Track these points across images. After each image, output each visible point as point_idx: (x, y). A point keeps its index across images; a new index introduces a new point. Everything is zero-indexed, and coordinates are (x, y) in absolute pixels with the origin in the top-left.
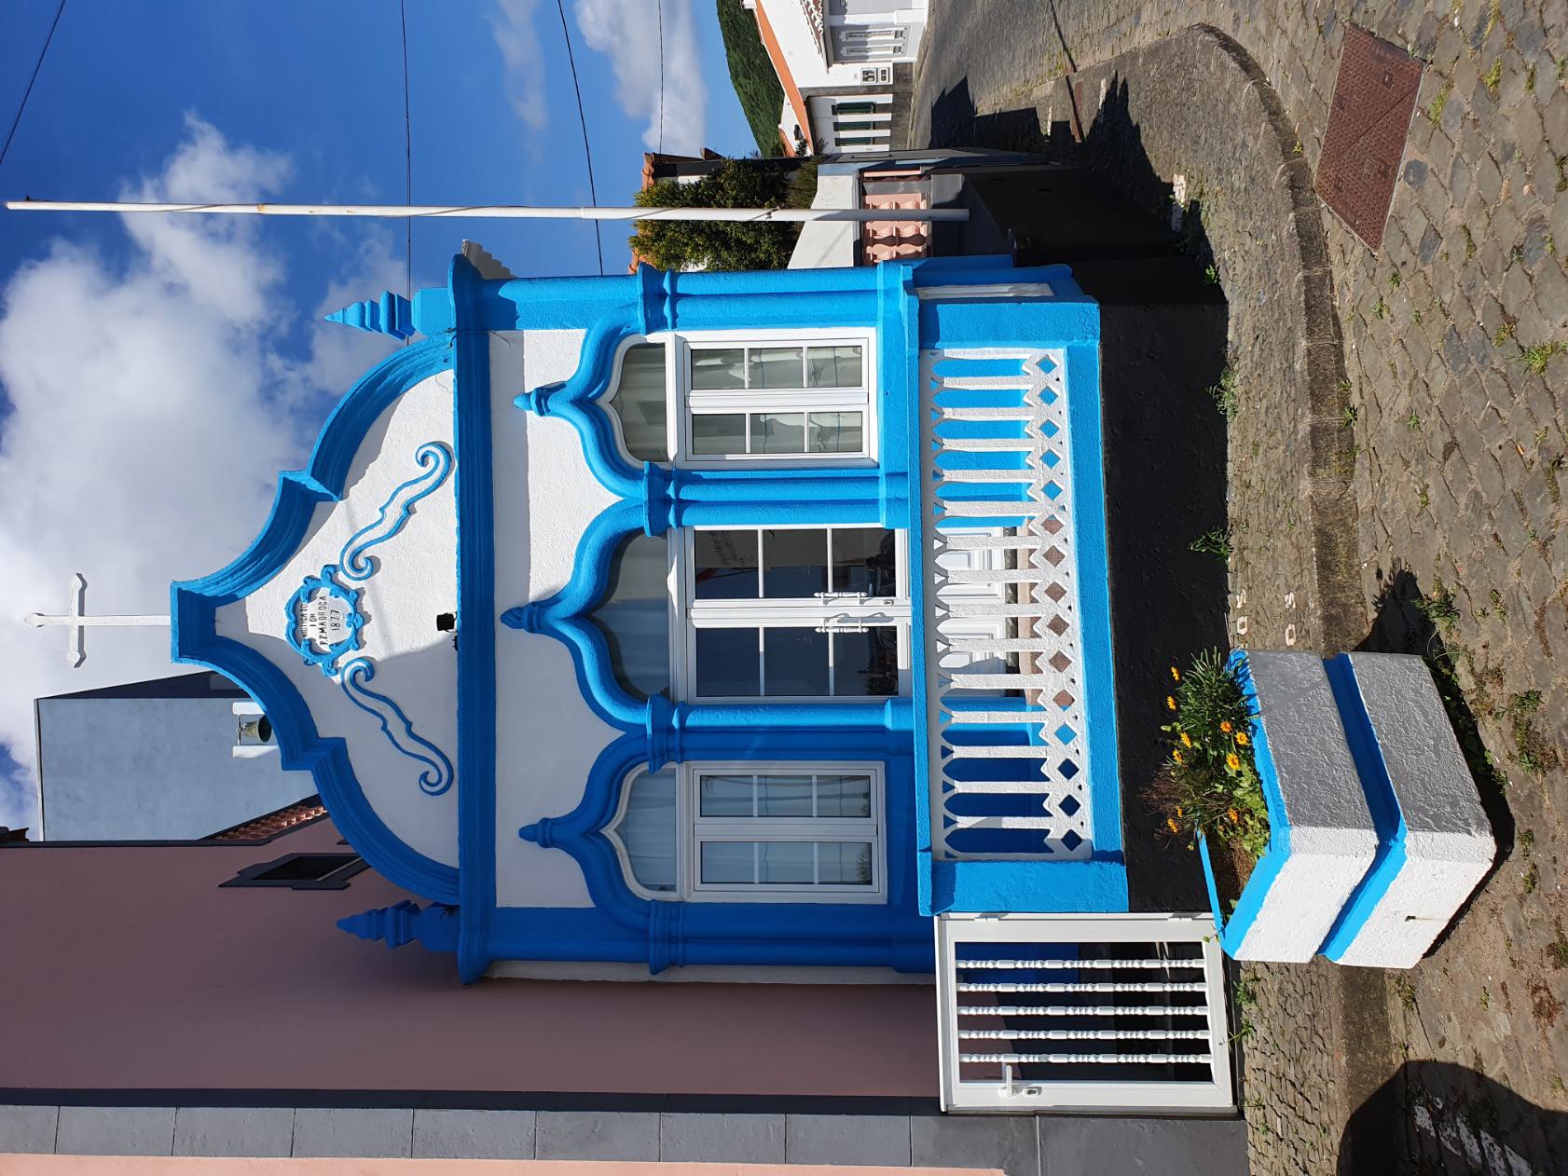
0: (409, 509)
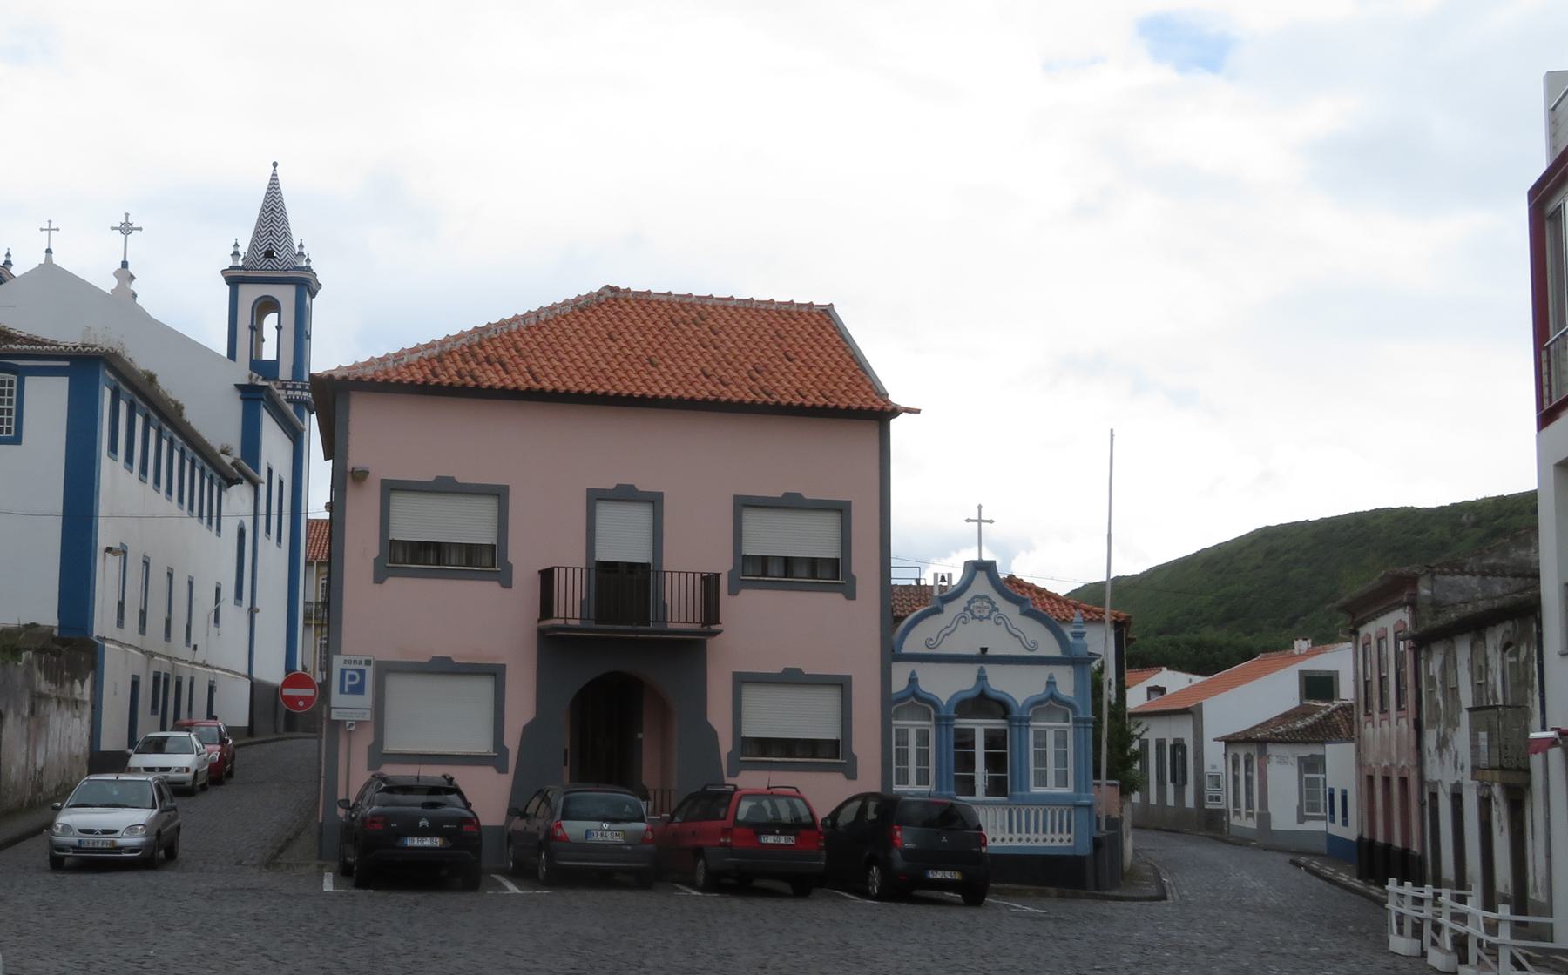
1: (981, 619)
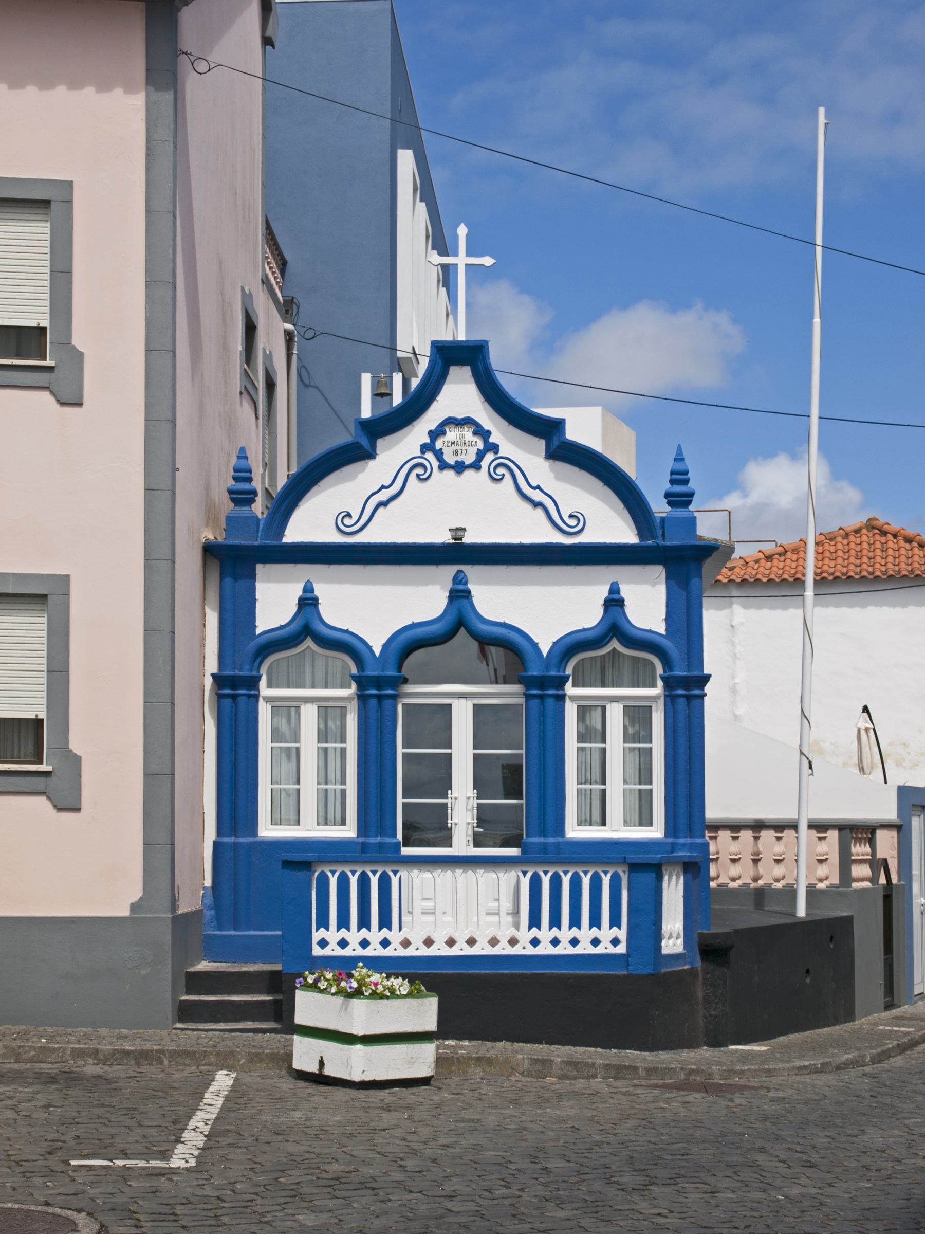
0: (537, 505)
1: (460, 468)
